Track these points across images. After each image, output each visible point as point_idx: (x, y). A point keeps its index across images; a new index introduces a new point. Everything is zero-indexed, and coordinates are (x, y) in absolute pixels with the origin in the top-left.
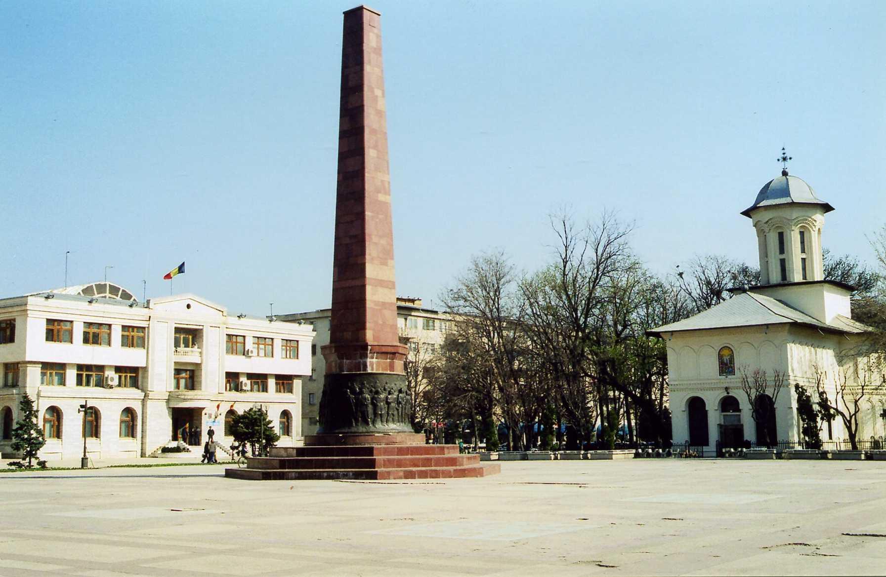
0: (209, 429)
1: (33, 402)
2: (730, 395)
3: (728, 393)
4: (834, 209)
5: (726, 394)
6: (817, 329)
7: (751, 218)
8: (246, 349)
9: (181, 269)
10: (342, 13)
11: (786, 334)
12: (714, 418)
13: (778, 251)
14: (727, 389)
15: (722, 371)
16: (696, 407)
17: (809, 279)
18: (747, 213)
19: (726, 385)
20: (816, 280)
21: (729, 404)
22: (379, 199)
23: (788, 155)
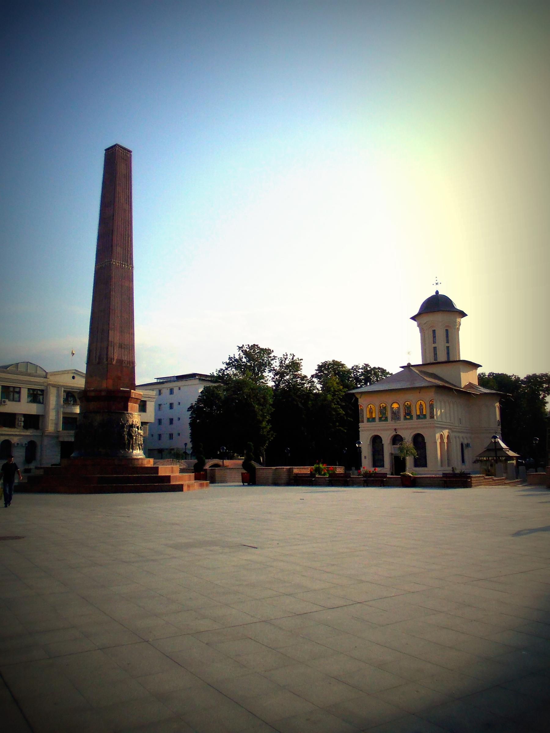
0: (229, 357)
1: (437, 292)
2: (397, 433)
3: (396, 433)
4: (467, 315)
5: (394, 433)
6: (453, 390)
7: (416, 321)
8: (155, 381)
9: (234, 355)
10: (104, 150)
11: (433, 393)
12: (388, 449)
13: (445, 341)
14: (395, 429)
15: (393, 418)
16: (376, 440)
17: (451, 359)
18: (413, 318)
19: (396, 427)
20: (457, 360)
21: (397, 439)
22: (456, 472)
23: (439, 282)
